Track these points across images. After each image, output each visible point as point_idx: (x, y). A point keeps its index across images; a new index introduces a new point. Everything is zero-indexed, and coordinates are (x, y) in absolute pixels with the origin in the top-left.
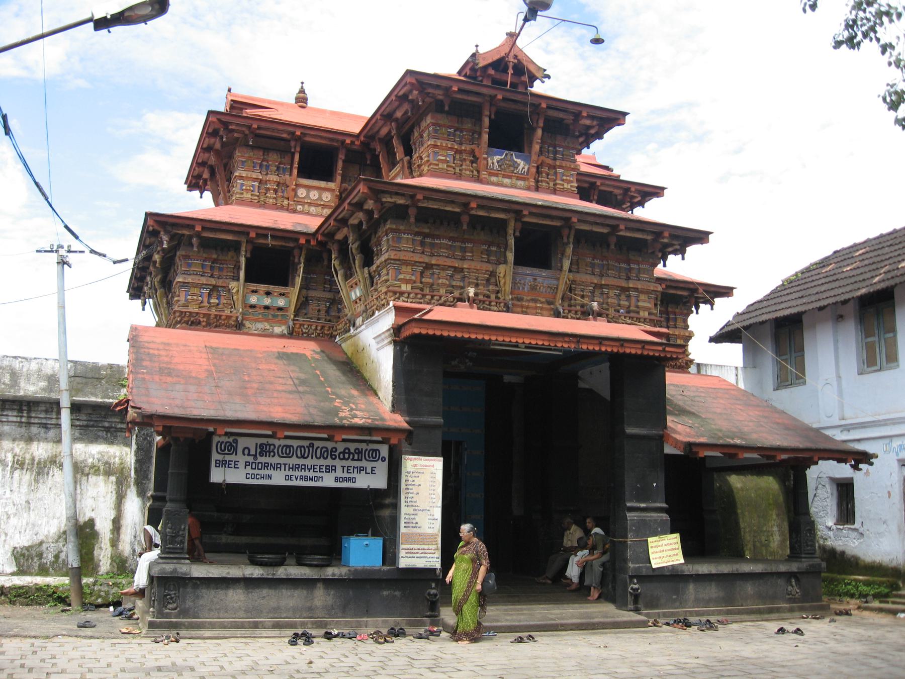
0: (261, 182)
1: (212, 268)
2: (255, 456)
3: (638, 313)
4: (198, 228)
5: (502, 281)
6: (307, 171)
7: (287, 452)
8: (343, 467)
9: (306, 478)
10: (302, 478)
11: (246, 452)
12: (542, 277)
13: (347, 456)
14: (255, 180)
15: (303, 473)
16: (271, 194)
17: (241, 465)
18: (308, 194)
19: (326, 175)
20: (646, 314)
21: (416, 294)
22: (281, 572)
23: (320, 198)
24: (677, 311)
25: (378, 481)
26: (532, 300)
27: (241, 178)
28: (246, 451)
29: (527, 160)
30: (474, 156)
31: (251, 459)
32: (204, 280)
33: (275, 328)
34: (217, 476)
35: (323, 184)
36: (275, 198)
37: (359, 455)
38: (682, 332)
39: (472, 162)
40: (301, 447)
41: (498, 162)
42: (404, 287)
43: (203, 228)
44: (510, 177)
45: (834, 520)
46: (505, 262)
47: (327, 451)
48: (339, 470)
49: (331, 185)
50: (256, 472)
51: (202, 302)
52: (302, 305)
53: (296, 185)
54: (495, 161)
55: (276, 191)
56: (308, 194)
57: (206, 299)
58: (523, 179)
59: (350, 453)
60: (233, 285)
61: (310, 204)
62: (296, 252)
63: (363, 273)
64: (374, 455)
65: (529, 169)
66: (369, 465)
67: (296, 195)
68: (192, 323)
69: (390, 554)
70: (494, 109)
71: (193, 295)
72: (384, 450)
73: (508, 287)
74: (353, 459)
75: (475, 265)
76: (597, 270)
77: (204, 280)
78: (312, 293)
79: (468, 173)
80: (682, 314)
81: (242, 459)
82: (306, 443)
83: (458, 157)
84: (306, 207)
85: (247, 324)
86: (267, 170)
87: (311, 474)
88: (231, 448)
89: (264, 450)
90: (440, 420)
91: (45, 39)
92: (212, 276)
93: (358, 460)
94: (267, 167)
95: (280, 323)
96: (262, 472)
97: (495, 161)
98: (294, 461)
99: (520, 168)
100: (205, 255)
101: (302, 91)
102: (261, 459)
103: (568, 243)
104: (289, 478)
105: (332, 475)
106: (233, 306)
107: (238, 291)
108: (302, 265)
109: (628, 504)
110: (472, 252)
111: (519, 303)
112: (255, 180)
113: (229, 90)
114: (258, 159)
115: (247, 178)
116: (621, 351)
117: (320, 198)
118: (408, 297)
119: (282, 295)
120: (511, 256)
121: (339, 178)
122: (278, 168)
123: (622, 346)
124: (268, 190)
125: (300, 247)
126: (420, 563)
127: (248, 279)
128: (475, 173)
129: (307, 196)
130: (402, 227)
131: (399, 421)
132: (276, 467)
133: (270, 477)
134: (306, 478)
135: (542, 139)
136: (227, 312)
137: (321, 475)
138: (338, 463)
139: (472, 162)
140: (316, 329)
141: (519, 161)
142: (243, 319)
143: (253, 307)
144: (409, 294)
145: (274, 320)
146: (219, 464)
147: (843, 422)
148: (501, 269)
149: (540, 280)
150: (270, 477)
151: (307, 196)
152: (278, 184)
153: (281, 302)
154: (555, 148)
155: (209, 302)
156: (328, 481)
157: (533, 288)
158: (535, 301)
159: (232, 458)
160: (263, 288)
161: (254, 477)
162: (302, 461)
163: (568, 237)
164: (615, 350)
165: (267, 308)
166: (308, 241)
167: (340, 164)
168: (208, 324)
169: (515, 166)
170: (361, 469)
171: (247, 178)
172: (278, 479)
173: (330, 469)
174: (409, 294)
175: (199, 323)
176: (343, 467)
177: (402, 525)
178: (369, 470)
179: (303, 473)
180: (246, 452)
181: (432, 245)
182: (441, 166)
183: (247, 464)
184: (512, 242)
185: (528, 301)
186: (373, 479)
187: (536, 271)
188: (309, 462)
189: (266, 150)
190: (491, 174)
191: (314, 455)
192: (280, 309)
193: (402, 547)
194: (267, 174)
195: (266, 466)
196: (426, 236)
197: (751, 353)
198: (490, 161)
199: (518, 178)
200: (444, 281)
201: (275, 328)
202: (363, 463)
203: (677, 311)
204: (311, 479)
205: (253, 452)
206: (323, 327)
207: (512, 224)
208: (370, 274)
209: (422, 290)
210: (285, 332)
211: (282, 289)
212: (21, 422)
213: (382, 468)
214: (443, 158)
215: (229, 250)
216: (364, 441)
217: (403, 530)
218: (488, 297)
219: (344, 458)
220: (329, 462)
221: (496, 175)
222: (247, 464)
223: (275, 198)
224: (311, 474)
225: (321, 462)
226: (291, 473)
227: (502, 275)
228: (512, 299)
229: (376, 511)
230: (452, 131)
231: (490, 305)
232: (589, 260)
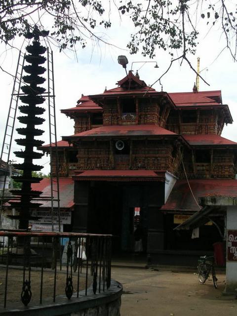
3: (161, 165)
6: (125, 111)
10: (47, 221)
19: (133, 111)
20: (164, 165)
37: (63, 215)
64: (68, 215)
66: (66, 218)
76: (146, 152)
90: (86, 204)
131: (141, 240)
149: (123, 158)
158: (124, 165)
160: (72, 164)
169: (131, 117)
194: (208, 122)
196: (88, 149)
218: (108, 165)
221: (125, 122)
228: (60, 162)
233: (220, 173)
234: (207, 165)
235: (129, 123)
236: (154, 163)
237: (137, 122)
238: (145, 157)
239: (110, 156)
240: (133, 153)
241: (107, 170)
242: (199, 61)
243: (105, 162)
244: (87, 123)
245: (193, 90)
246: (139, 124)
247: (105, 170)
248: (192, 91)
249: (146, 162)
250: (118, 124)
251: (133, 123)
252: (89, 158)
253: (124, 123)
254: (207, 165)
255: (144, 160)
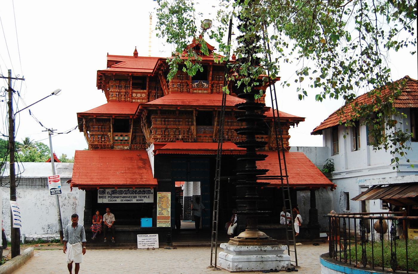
0: (119, 92)
1: (101, 128)
2: (111, 195)
4: (95, 116)
5: (193, 131)
7: (121, 193)
8: (139, 196)
9: (127, 200)
11: (108, 193)
12: (208, 128)
13: (140, 193)
14: (117, 92)
15: (126, 199)
16: (123, 97)
17: (107, 197)
18: (137, 95)
21: (162, 139)
22: (266, 249)
23: (141, 96)
24: (283, 128)
25: (150, 200)
26: (204, 136)
27: (111, 92)
28: (108, 193)
29: (207, 83)
30: (187, 84)
31: (110, 195)
32: (99, 133)
33: (125, 147)
34: (100, 201)
35: (142, 91)
36: (125, 98)
37: (144, 192)
38: (285, 136)
39: (187, 86)
40: (125, 191)
41: (196, 85)
42: (158, 137)
43: (96, 116)
44: (201, 90)
45: (346, 209)
46: (193, 125)
47: (134, 192)
48: (138, 197)
49: (145, 91)
50: (112, 199)
51: (99, 140)
52: (134, 138)
53: (132, 93)
54: (195, 85)
55: (125, 95)
56: (137, 95)
57: (100, 139)
58: (207, 90)
59: (141, 192)
60: (109, 134)
61: (138, 99)
62: (130, 121)
63: (148, 130)
64: (149, 192)
65: (208, 86)
66: (147, 195)
67: (132, 96)
68: (96, 148)
69: (154, 223)
71: (95, 138)
72: (152, 191)
73: (195, 133)
74: (142, 194)
75: (182, 127)
77: (99, 133)
78: (137, 134)
79: (185, 90)
80: (285, 129)
81: (107, 195)
82: (127, 189)
83: (182, 85)
84: (136, 100)
85: (115, 147)
86: (121, 87)
87: (129, 199)
88: (104, 192)
89: (114, 192)
92: (102, 131)
93: (144, 194)
94: (121, 86)
95: (126, 146)
96: (113, 199)
97: (195, 85)
98: (123, 195)
99: (205, 86)
100: (99, 124)
101: (136, 50)
102: (113, 195)
103: (216, 116)
104: (122, 200)
105: (136, 199)
106: (109, 141)
107: (111, 136)
108: (132, 125)
109: (239, 205)
110: (182, 122)
111: (200, 138)
112: (117, 92)
113: (108, 54)
114: (117, 84)
115: (114, 92)
116: (231, 154)
117: (141, 96)
118: (160, 140)
119: (126, 136)
120: (195, 123)
121: (147, 88)
122: (125, 86)
123: (232, 152)
124: (122, 95)
125: (131, 119)
126: (164, 226)
127: (114, 131)
128: (188, 90)
129: (136, 96)
130: (157, 117)
132: (118, 197)
133: (116, 201)
134: (127, 200)
135: (212, 75)
136: (108, 143)
137: (132, 199)
138: (137, 195)
139: (187, 86)
140: (139, 146)
141: (204, 84)
142: (113, 145)
144: (160, 139)
145: (124, 145)
146: (100, 197)
147: (370, 167)
148: (192, 127)
150: (116, 201)
151: (136, 96)
152: (126, 92)
153: (126, 138)
154: (219, 76)
155: (101, 140)
156: (134, 201)
157: (204, 133)
158: (206, 137)
159: (104, 195)
160: (119, 134)
162: (126, 195)
163: (216, 115)
164: (229, 154)
165: (121, 140)
166: (133, 117)
167: (147, 83)
168: (101, 148)
169: (203, 85)
170: (145, 197)
171: (114, 92)
172: (119, 201)
173: (135, 197)
174: (160, 139)
175: (98, 148)
176: (139, 196)
177: (158, 214)
178: (147, 197)
179: (126, 199)
180: (108, 193)
181: (168, 121)
182: (175, 89)
183: (109, 197)
184: (195, 118)
185: (203, 137)
186: (148, 200)
187: (205, 127)
188: (128, 195)
189: (120, 80)
190: (194, 90)
191: (130, 193)
192: (126, 140)
193: (157, 221)
194: (121, 89)
195: (114, 197)
196: (165, 118)
197: (325, 139)
198: (193, 85)
199: (204, 90)
200: (172, 133)
201: (125, 147)
202: (146, 195)
203: (283, 128)
204: (129, 201)
205: (110, 193)
206: (141, 146)
207: (194, 112)
208: (150, 130)
209: (165, 137)
210: (128, 148)
213: (152, 196)
214: (176, 86)
215: (107, 122)
216: (143, 188)
217: (158, 215)
218: (189, 137)
219: (139, 194)
220: (134, 195)
221: (196, 90)
222: (109, 197)
223: (125, 98)
224: (129, 199)
225: (132, 195)
226: (122, 199)
227: (193, 129)
230: (179, 75)
231: (188, 140)
232: (226, 120)
233: (103, 143)
234: (266, 138)
235: (200, 91)
236: (175, 134)
237: (210, 91)
238: (229, 129)
239: (192, 127)
240: (218, 125)
241: (189, 142)
242: (151, 18)
243: (186, 134)
244: (125, 87)
245: (134, 54)
246: (212, 93)
247: (186, 142)
248: (133, 55)
249: (230, 134)
250: (188, 92)
251: (205, 92)
252: (167, 129)
253: (195, 91)
254: (266, 138)
255: (228, 132)
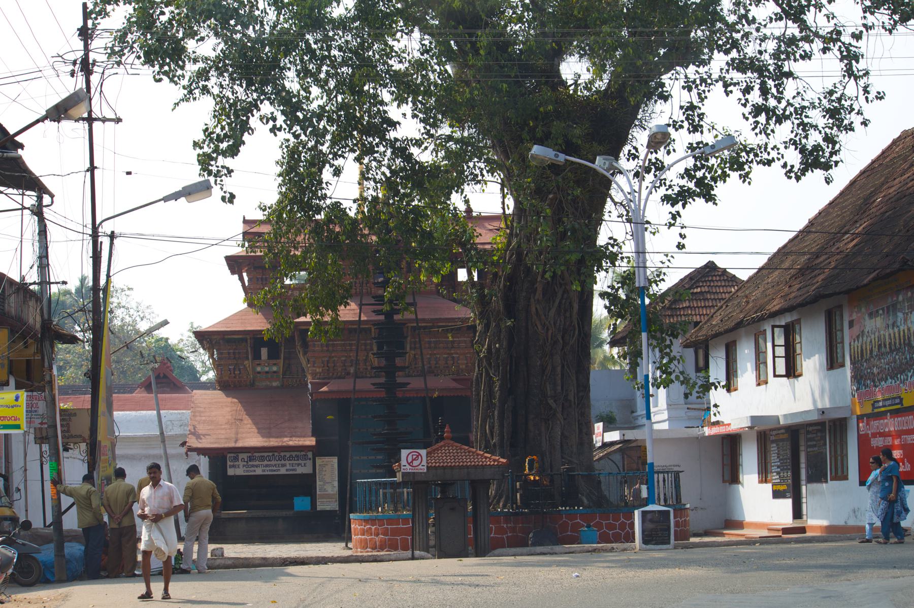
17: (241, 466)
34: (231, 472)
66: (303, 462)
69: (314, 503)
70: (89, 518)
81: (241, 463)
87: (275, 468)
89: (251, 459)
91: (194, 606)
98: (266, 462)
102: (250, 463)
105: (285, 468)
119: (274, 364)
126: (328, 508)
132: (257, 466)
138: (287, 462)
143: (259, 373)
146: (231, 467)
153: (275, 369)
161: (247, 471)
165: (267, 372)
170: (299, 465)
172: (259, 472)
173: (283, 465)
186: (306, 469)
188: (273, 463)
192: (275, 372)
195: (253, 466)
202: (300, 462)
211: (274, 361)
212: (423, 374)
213: (309, 463)
220: (283, 462)
224: (275, 468)
225: (279, 462)
229: (306, 485)
